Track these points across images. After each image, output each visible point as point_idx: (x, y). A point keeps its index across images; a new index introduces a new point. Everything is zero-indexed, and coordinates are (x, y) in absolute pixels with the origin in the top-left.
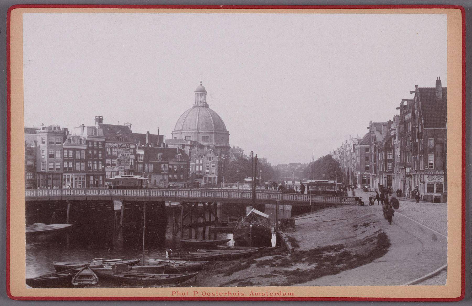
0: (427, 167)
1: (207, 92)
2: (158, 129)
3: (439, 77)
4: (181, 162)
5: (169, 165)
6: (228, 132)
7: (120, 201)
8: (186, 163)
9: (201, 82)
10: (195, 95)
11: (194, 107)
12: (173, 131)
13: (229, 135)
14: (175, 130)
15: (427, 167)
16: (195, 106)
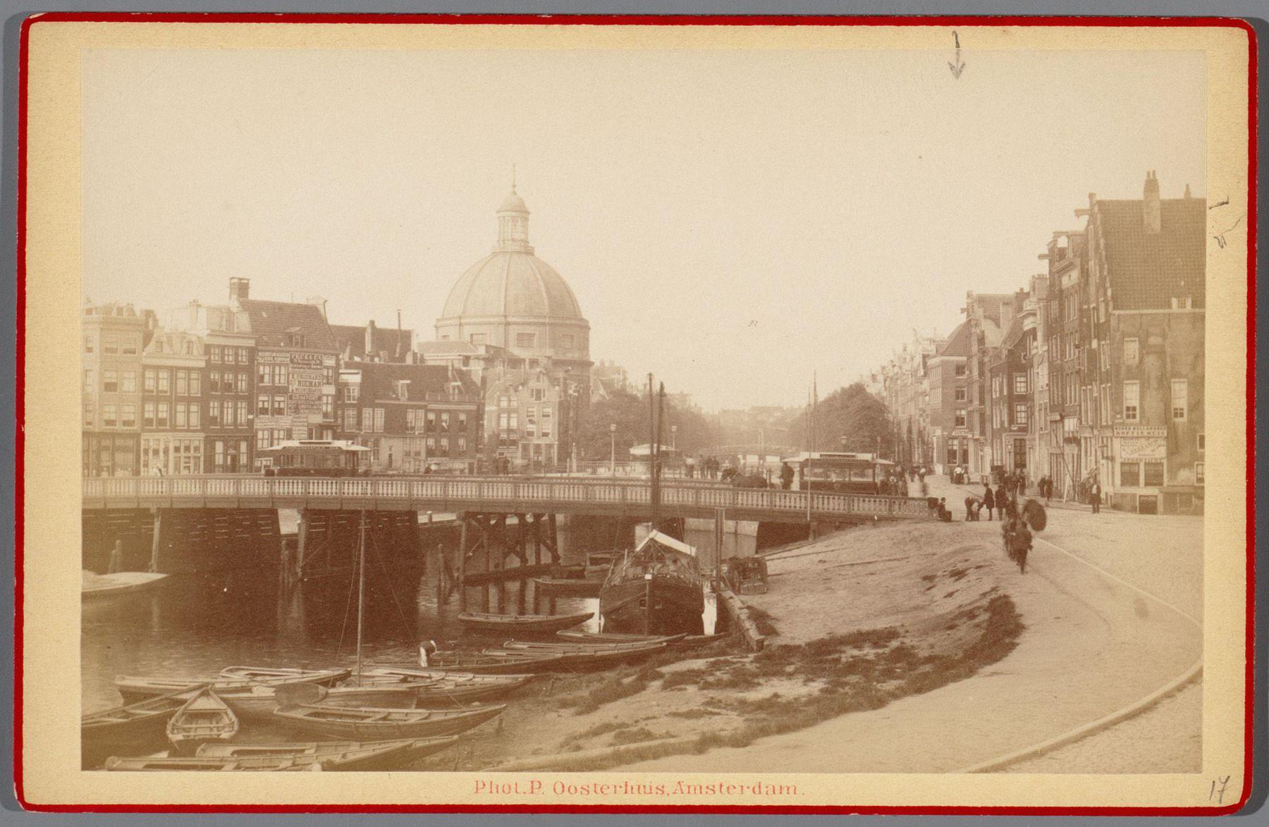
3: (1154, 172)
4: (459, 403)
5: (427, 411)
8: (473, 407)
11: (495, 254)
15: (1122, 418)
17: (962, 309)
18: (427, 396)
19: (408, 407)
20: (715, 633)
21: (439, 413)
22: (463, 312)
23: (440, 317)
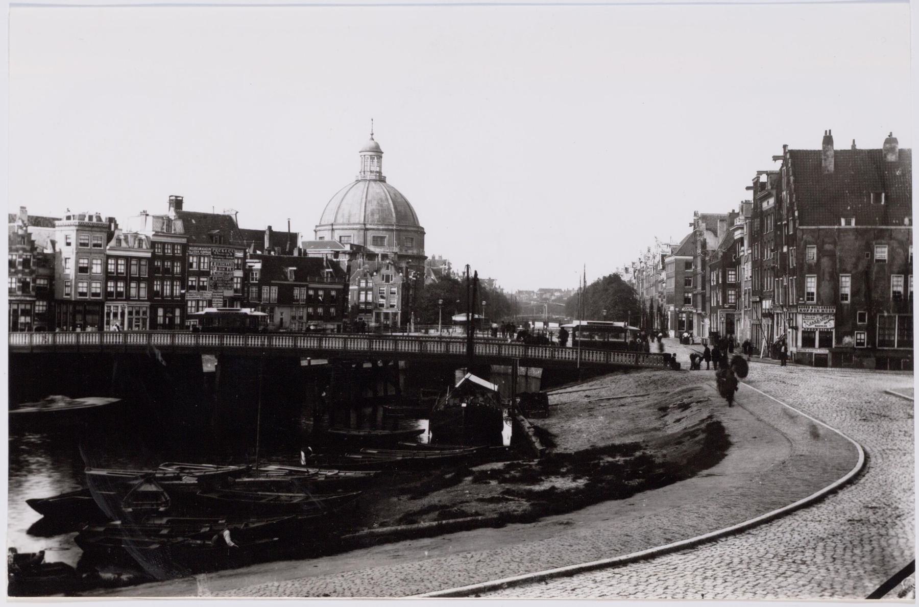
1: (382, 153)
2: (289, 222)
3: (830, 131)
4: (331, 283)
5: (308, 289)
6: (423, 228)
11: (358, 181)
12: (317, 226)
21: (316, 290)
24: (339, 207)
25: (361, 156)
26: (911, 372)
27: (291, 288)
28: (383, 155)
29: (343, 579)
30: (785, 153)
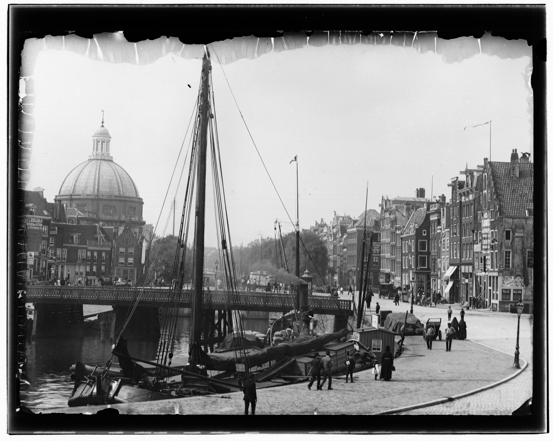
0: (503, 267)
1: (111, 138)
2: (298, 218)
3: (516, 150)
4: (103, 246)
5: (87, 250)
6: (142, 199)
7: (255, 341)
8: (109, 249)
9: (103, 123)
10: (93, 141)
11: (90, 160)
12: (56, 196)
13: (143, 203)
14: (59, 194)
15: (503, 267)
16: (92, 158)
17: (379, 204)
18: (87, 242)
19: (78, 248)
20: (334, 332)
21: (92, 252)
22: (73, 193)
23: (58, 195)
24: (76, 181)
25: (94, 140)
26: (512, 308)
27: (76, 250)
28: (111, 140)
29: (476, 407)
30: (485, 163)
